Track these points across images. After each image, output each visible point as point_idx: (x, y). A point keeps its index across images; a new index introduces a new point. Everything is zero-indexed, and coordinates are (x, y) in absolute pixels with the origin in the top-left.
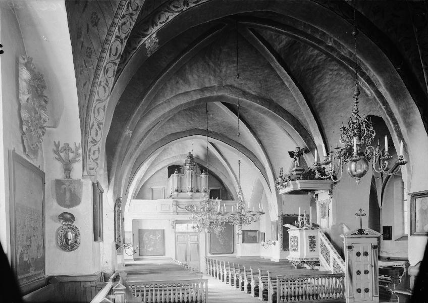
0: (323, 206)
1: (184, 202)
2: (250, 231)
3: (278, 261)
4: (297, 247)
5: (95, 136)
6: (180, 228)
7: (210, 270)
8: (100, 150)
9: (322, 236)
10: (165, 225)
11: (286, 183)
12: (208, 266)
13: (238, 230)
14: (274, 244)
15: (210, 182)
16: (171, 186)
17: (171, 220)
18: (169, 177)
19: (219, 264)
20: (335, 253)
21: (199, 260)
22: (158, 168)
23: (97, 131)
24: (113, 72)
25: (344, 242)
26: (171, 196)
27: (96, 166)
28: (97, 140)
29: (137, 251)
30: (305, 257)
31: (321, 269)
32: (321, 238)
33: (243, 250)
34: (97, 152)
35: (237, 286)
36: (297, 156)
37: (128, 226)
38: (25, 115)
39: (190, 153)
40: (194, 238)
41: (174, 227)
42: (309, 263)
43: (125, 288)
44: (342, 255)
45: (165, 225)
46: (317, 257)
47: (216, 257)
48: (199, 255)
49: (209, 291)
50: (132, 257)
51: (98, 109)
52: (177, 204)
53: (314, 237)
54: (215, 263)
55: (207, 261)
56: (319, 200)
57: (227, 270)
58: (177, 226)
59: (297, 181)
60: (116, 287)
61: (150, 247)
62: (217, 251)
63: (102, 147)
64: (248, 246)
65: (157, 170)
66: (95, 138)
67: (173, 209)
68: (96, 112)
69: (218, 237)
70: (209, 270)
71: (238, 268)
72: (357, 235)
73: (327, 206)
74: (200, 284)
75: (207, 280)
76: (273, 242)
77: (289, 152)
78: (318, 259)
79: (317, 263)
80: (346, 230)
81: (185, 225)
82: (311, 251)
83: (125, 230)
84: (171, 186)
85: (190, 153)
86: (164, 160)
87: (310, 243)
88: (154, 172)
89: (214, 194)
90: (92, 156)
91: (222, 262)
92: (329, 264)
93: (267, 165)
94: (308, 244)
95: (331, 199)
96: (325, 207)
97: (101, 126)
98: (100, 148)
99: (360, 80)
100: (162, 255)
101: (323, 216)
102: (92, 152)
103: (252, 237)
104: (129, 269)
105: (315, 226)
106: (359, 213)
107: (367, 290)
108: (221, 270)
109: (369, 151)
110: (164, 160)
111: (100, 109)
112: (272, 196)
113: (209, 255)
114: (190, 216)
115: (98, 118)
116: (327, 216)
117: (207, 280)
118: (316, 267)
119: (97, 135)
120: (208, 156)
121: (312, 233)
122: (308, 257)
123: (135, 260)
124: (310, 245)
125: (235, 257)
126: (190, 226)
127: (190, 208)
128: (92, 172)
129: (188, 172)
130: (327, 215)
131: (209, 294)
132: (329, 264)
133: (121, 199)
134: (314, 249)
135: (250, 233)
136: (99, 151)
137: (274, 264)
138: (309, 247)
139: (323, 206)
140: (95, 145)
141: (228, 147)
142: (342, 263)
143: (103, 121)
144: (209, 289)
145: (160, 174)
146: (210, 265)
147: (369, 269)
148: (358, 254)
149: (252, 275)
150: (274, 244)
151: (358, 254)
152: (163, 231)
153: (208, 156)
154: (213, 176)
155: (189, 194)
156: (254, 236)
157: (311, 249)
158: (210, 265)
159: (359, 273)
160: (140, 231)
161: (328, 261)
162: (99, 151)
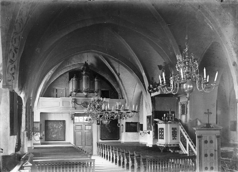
0: (183, 106)
1: (81, 100)
2: (132, 123)
3: (151, 146)
4: (163, 136)
5: (12, 57)
6: (79, 119)
7: (100, 153)
8: (16, 67)
9: (181, 128)
10: (66, 117)
11: (155, 89)
12: (99, 149)
13: (123, 122)
14: (149, 133)
15: (100, 83)
16: (71, 88)
17: (70, 114)
18: (70, 80)
19: (107, 148)
20: (190, 141)
21: (92, 144)
22: (61, 73)
23: (14, 54)
25: (196, 133)
26: (71, 95)
27: (13, 79)
28: (14, 61)
29: (44, 138)
30: (169, 144)
31: (181, 153)
32: (181, 129)
33: (126, 137)
34: (13, 69)
36: (164, 69)
37: (37, 118)
38: (17, 145)
39: (86, 62)
40: (88, 127)
41: (73, 119)
42: (172, 148)
43: (31, 165)
44: (194, 142)
45: (66, 117)
47: (106, 143)
48: (92, 141)
49: (95, 166)
50: (39, 142)
51: (15, 39)
52: (75, 101)
53: (176, 129)
54: (104, 147)
55: (98, 145)
56: (181, 101)
57: (113, 153)
58: (76, 118)
60: (25, 165)
61: (53, 134)
62: (106, 138)
63: (18, 65)
64: (130, 134)
65: (62, 73)
66: (12, 59)
67: (71, 105)
68: (13, 40)
69: (107, 127)
71: (120, 151)
72: (205, 128)
75: (95, 160)
76: (148, 131)
77: (158, 66)
78: (178, 145)
79: (178, 148)
80: (199, 123)
81: (82, 117)
82: (173, 139)
83: (34, 121)
84: (71, 88)
85: (86, 62)
86: (66, 67)
87: (172, 133)
88: (58, 76)
89: (104, 94)
90: (10, 71)
93: (144, 74)
94: (171, 134)
95: (189, 101)
97: (17, 50)
98: (16, 66)
100: (63, 141)
101: (183, 113)
102: (10, 69)
103: (133, 127)
104: (36, 151)
105: (177, 121)
106: (207, 112)
109: (194, 76)
110: (66, 67)
111: (17, 39)
112: (148, 96)
113: (100, 141)
114: (85, 111)
115: (15, 45)
117: (95, 160)
118: (178, 151)
119: (13, 57)
120: (99, 63)
121: (174, 126)
122: (170, 144)
123: (42, 144)
124: (173, 135)
125: (120, 142)
126: (85, 118)
127: (85, 105)
128: (10, 83)
129: (84, 77)
131: (95, 168)
132: (186, 150)
133: (31, 98)
134: (176, 138)
135: (131, 124)
136: (15, 68)
137: (148, 148)
138: (171, 136)
139: (183, 106)
140: (12, 64)
142: (195, 148)
143: (19, 47)
145: (63, 78)
146: (100, 148)
147: (213, 152)
149: (129, 157)
150: (149, 133)
151: (206, 142)
152: (64, 122)
153: (99, 63)
154: (102, 80)
155: (85, 94)
156: (134, 127)
157: (173, 138)
158: (100, 148)
159: (206, 155)
160: (47, 122)
161: (185, 147)
162: (15, 68)
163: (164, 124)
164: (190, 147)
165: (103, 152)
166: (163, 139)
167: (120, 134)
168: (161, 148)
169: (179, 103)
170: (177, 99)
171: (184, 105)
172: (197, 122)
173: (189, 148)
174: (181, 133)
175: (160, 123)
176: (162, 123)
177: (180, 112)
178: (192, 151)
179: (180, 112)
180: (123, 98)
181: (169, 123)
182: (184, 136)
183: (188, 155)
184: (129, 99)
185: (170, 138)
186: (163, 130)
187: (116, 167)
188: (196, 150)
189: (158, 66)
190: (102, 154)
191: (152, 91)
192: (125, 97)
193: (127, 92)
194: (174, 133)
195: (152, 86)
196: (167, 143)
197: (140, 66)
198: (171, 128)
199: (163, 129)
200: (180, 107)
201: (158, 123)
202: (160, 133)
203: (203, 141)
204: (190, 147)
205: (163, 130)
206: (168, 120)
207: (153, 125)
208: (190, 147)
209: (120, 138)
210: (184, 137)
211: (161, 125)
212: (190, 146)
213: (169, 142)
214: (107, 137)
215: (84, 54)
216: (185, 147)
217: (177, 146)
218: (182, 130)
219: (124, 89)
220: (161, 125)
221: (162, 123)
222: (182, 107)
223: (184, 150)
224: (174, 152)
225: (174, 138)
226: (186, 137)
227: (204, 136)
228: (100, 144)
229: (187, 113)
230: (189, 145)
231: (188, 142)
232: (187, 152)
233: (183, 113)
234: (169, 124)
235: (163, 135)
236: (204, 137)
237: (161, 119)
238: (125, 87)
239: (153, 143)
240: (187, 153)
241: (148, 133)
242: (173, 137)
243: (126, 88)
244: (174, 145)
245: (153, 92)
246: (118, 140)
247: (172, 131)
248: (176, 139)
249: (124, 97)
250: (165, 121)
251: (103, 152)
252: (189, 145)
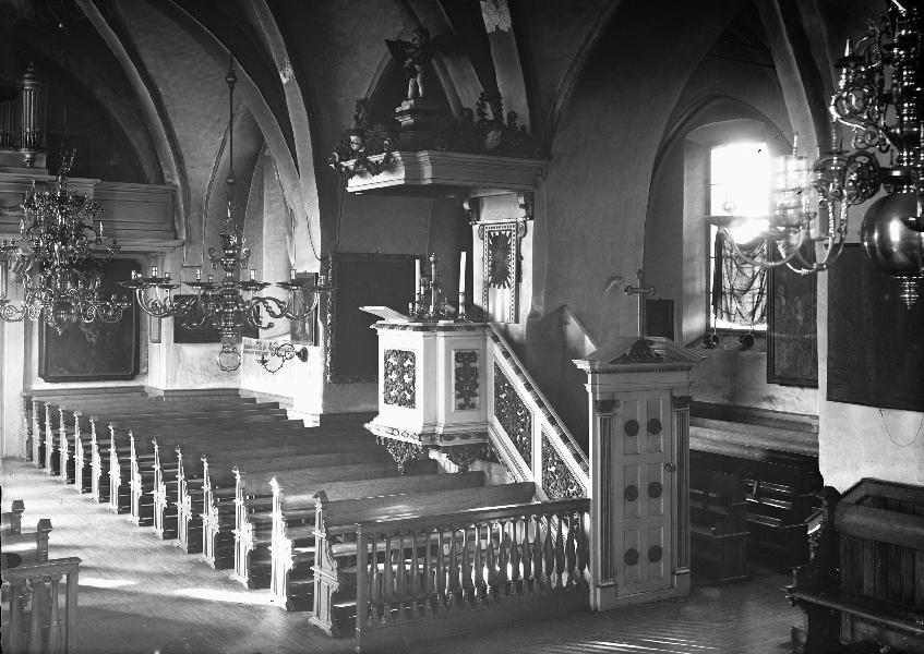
14: (303, 355)
20: (552, 420)
24: (284, 214)
30: (440, 430)
35: (105, 496)
44: (575, 431)
46: (480, 428)
55: (28, 406)
56: (483, 220)
59: (424, 156)
64: (192, 351)
70: (36, 445)
73: (512, 243)
74: (510, 567)
76: (298, 348)
77: (387, 41)
78: (485, 435)
91: (69, 414)
92: (528, 462)
95: (531, 223)
96: (508, 248)
99: (652, 343)
101: (498, 276)
105: (479, 318)
107: (655, 554)
108: (64, 443)
113: (40, 384)
116: (512, 280)
121: (467, 342)
124: (458, 387)
130: (512, 270)
132: (528, 462)
139: (499, 244)
141: (280, 138)
142: (579, 459)
144: (24, 529)
148: (654, 427)
150: (303, 355)
157: (462, 401)
161: (525, 451)
163: (420, 334)
164: (549, 453)
165: (49, 444)
166: (411, 404)
167: (142, 349)
168: (395, 450)
169: (475, 228)
170: (466, 206)
171: (506, 239)
172: (566, 323)
173: (545, 455)
174: (501, 378)
175: (393, 327)
176: (405, 327)
177: (480, 272)
178: (565, 473)
179: (480, 272)
180: (161, 180)
181: (445, 329)
182: (515, 394)
183: (542, 497)
184: (193, 186)
185: (448, 404)
186: (413, 360)
187: (147, 543)
188: (586, 470)
189: (387, 41)
190: (42, 449)
191: (357, 165)
192: (171, 176)
193: (183, 149)
194: (467, 379)
195: (363, 141)
196: (429, 430)
197: (272, 33)
198: (453, 353)
199: (405, 355)
200: (479, 249)
201: (382, 326)
202: (394, 376)
203: (618, 425)
204: (554, 452)
205: (408, 362)
206: (438, 317)
207: (324, 320)
208: (549, 453)
209: (144, 370)
210: (514, 398)
211: (395, 336)
212: (549, 444)
213: (442, 419)
214: (75, 366)
215: (521, 76)
216: (525, 451)
217: (481, 440)
218: (509, 371)
219: (171, 137)
220: (395, 336)
221: (405, 327)
222: (490, 247)
223: (519, 468)
224: (464, 470)
225: (467, 400)
226: (528, 398)
227: (622, 402)
228: (41, 405)
229: (519, 279)
230: (545, 439)
231: (541, 423)
232: (535, 476)
233: (498, 276)
234: (442, 334)
235: (410, 388)
236: (622, 407)
237: (404, 311)
238: (174, 125)
239: (324, 407)
240: (531, 479)
241: (298, 354)
242: (458, 397)
243: (178, 132)
244: (465, 436)
245: (362, 175)
246: (132, 378)
247: (458, 365)
248: (473, 406)
249: (166, 172)
250: (420, 318)
251: (49, 444)
252: (545, 439)
